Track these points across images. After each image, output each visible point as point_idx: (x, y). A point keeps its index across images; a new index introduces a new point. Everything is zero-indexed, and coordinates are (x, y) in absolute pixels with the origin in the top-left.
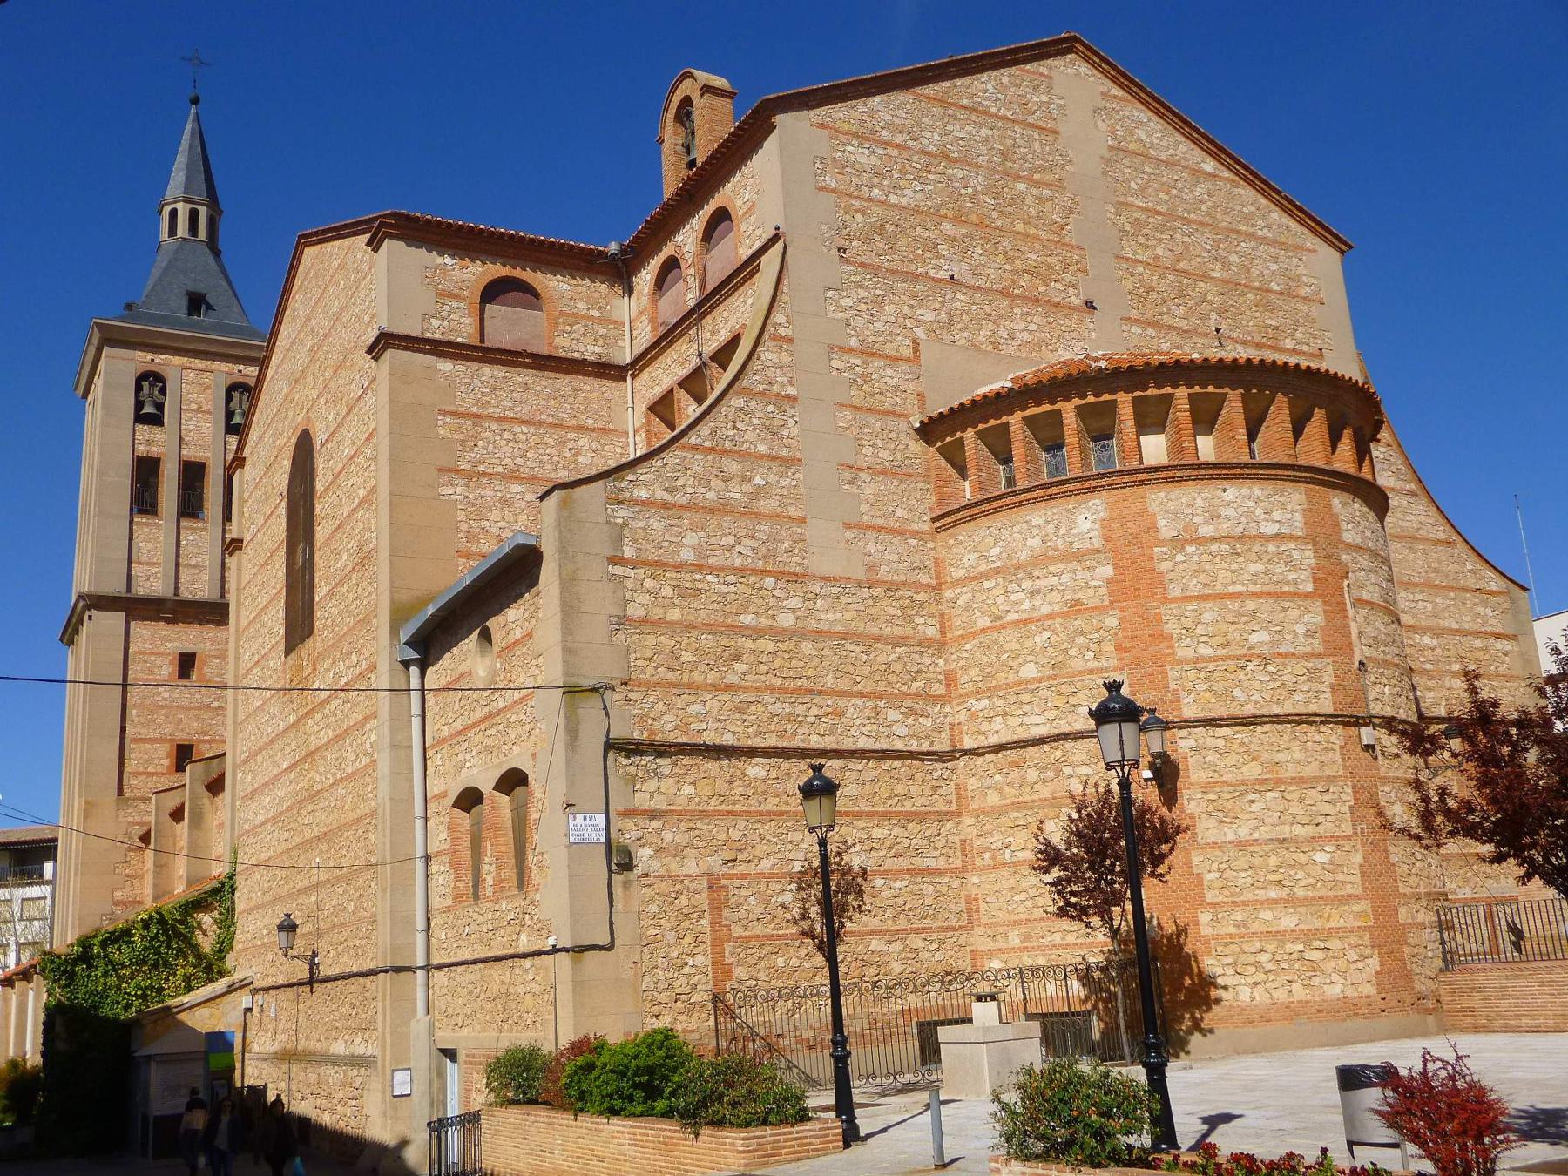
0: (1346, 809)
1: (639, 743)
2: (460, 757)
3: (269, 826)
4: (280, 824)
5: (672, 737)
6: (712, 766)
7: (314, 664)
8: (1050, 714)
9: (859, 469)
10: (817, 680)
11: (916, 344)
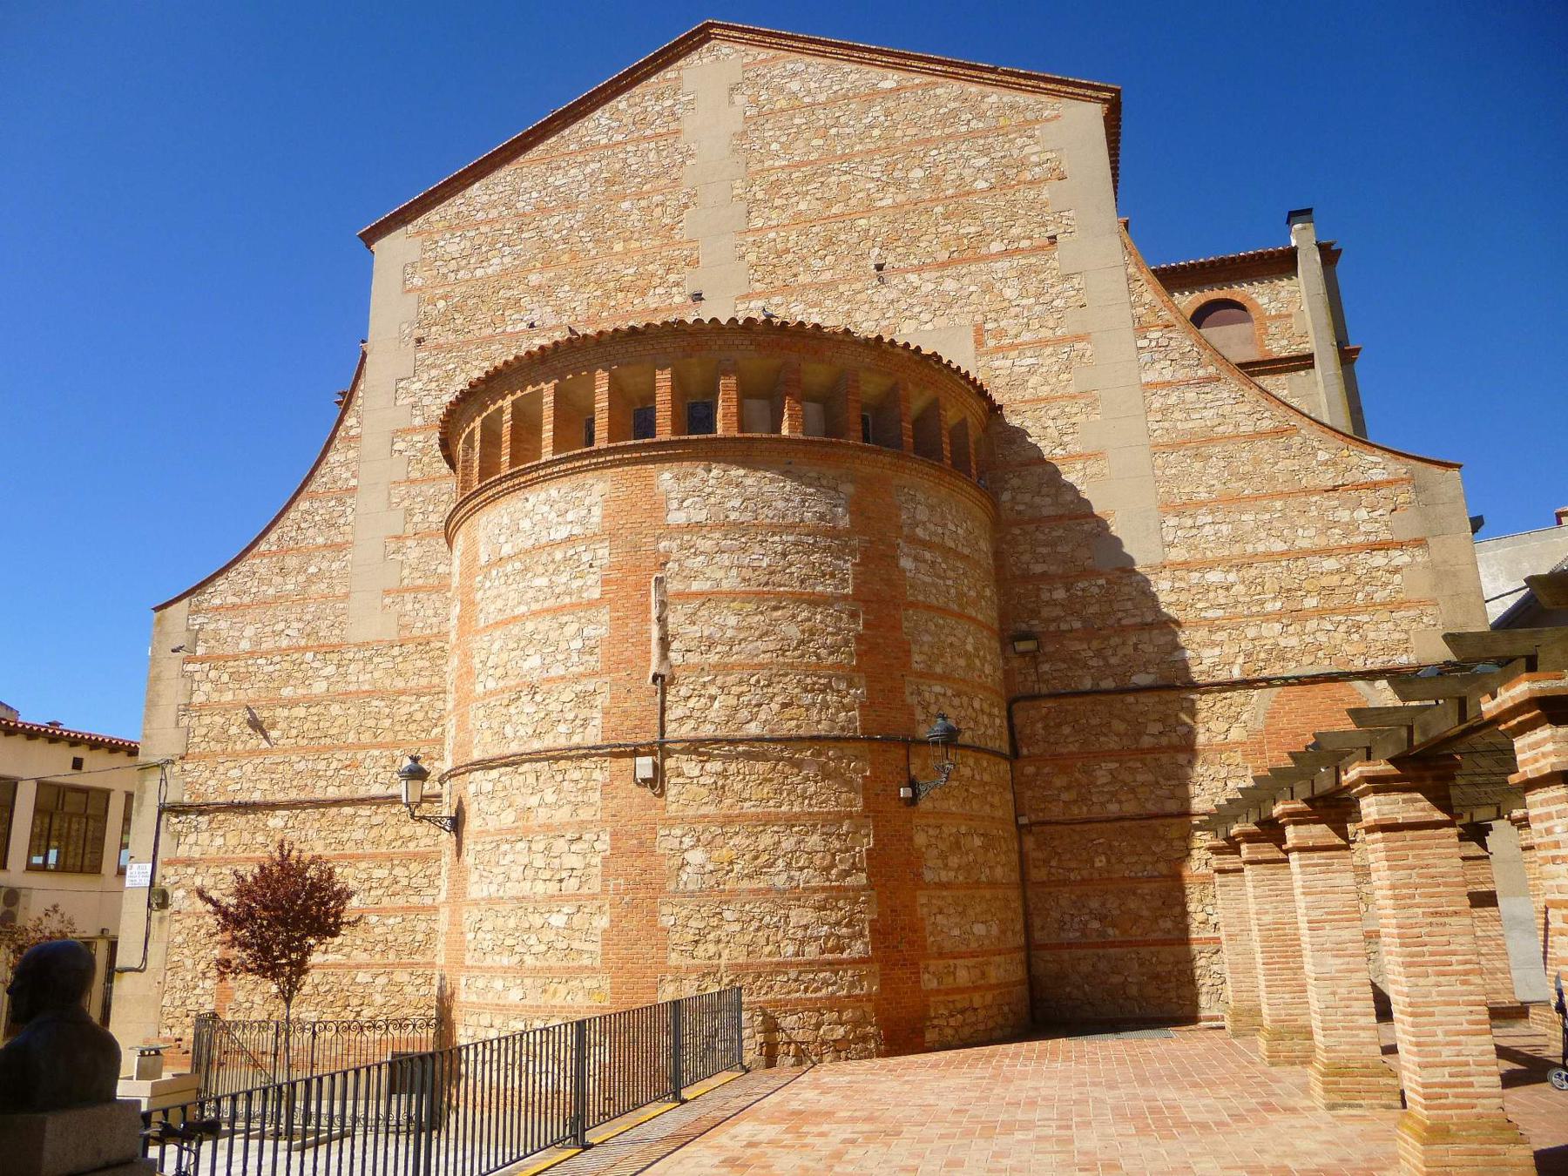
0: (597, 860)
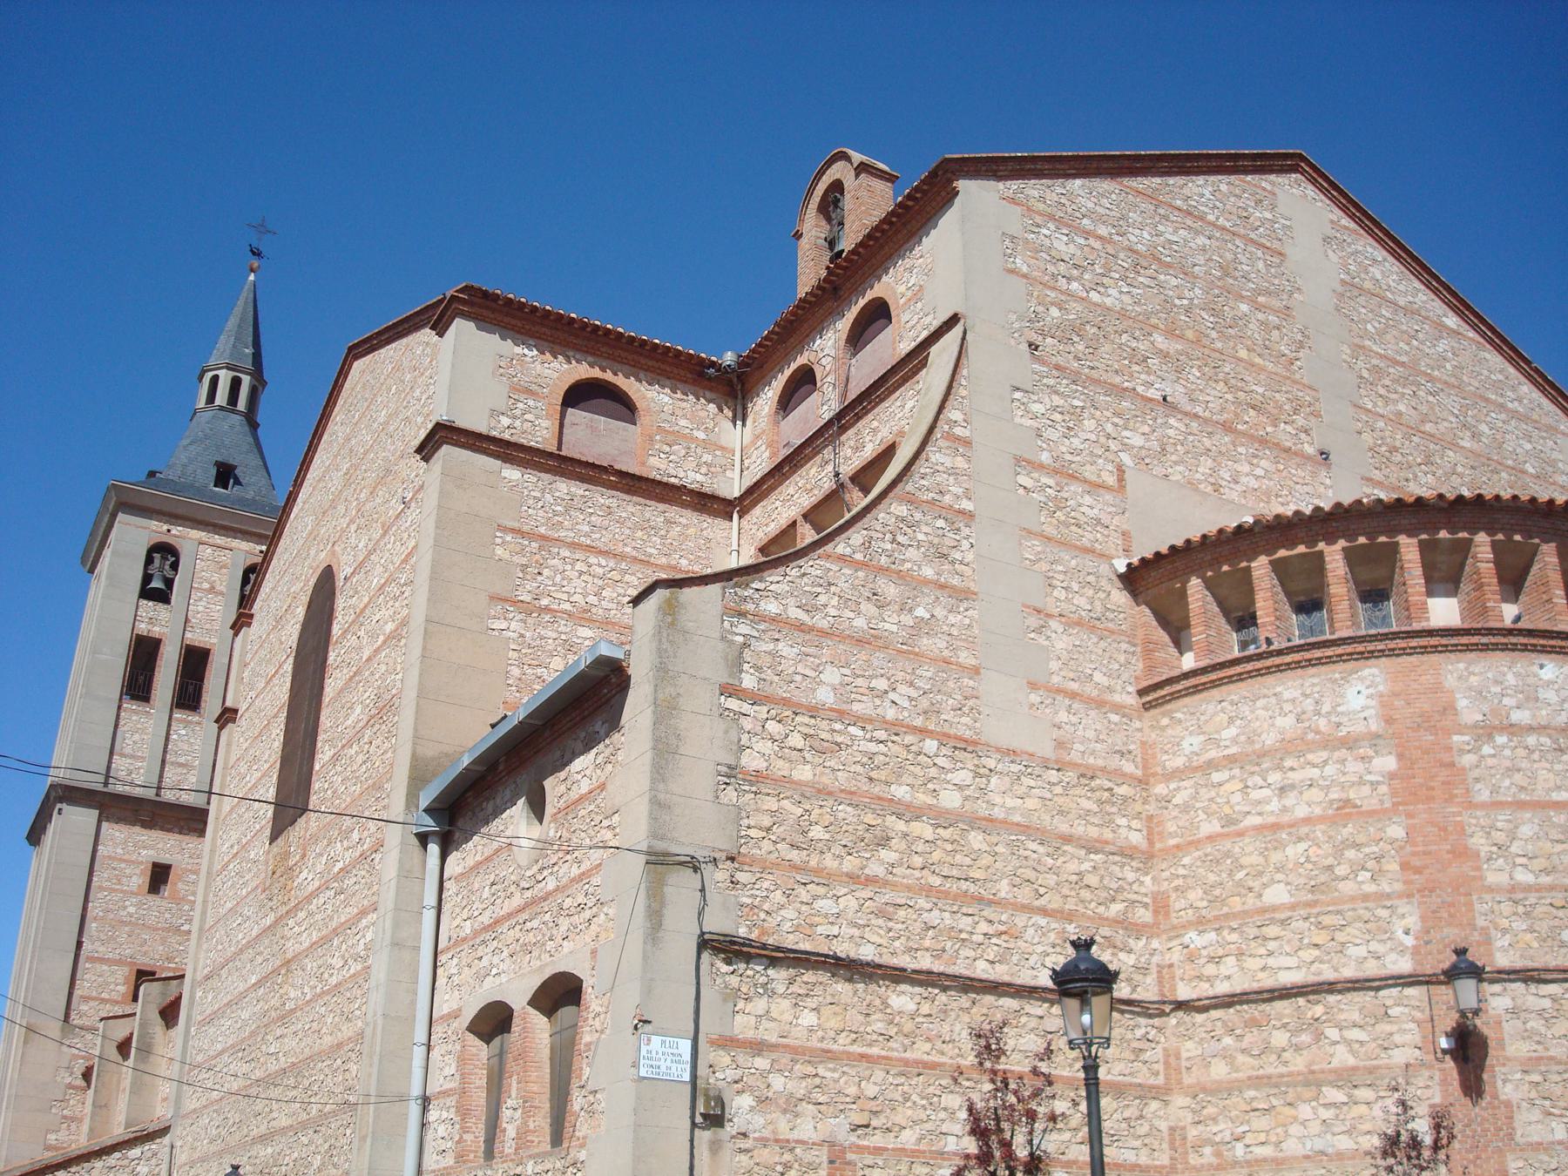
1: (748, 942)
2: (485, 962)
3: (225, 1057)
4: (240, 1054)
5: (790, 942)
6: (842, 988)
7: (304, 849)
8: (1309, 954)
9: (1049, 616)
10: (989, 885)
11: (1121, 470)
